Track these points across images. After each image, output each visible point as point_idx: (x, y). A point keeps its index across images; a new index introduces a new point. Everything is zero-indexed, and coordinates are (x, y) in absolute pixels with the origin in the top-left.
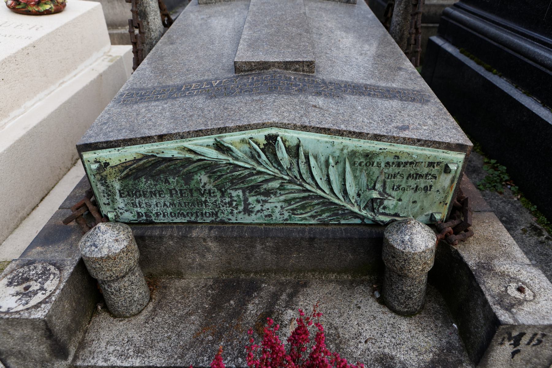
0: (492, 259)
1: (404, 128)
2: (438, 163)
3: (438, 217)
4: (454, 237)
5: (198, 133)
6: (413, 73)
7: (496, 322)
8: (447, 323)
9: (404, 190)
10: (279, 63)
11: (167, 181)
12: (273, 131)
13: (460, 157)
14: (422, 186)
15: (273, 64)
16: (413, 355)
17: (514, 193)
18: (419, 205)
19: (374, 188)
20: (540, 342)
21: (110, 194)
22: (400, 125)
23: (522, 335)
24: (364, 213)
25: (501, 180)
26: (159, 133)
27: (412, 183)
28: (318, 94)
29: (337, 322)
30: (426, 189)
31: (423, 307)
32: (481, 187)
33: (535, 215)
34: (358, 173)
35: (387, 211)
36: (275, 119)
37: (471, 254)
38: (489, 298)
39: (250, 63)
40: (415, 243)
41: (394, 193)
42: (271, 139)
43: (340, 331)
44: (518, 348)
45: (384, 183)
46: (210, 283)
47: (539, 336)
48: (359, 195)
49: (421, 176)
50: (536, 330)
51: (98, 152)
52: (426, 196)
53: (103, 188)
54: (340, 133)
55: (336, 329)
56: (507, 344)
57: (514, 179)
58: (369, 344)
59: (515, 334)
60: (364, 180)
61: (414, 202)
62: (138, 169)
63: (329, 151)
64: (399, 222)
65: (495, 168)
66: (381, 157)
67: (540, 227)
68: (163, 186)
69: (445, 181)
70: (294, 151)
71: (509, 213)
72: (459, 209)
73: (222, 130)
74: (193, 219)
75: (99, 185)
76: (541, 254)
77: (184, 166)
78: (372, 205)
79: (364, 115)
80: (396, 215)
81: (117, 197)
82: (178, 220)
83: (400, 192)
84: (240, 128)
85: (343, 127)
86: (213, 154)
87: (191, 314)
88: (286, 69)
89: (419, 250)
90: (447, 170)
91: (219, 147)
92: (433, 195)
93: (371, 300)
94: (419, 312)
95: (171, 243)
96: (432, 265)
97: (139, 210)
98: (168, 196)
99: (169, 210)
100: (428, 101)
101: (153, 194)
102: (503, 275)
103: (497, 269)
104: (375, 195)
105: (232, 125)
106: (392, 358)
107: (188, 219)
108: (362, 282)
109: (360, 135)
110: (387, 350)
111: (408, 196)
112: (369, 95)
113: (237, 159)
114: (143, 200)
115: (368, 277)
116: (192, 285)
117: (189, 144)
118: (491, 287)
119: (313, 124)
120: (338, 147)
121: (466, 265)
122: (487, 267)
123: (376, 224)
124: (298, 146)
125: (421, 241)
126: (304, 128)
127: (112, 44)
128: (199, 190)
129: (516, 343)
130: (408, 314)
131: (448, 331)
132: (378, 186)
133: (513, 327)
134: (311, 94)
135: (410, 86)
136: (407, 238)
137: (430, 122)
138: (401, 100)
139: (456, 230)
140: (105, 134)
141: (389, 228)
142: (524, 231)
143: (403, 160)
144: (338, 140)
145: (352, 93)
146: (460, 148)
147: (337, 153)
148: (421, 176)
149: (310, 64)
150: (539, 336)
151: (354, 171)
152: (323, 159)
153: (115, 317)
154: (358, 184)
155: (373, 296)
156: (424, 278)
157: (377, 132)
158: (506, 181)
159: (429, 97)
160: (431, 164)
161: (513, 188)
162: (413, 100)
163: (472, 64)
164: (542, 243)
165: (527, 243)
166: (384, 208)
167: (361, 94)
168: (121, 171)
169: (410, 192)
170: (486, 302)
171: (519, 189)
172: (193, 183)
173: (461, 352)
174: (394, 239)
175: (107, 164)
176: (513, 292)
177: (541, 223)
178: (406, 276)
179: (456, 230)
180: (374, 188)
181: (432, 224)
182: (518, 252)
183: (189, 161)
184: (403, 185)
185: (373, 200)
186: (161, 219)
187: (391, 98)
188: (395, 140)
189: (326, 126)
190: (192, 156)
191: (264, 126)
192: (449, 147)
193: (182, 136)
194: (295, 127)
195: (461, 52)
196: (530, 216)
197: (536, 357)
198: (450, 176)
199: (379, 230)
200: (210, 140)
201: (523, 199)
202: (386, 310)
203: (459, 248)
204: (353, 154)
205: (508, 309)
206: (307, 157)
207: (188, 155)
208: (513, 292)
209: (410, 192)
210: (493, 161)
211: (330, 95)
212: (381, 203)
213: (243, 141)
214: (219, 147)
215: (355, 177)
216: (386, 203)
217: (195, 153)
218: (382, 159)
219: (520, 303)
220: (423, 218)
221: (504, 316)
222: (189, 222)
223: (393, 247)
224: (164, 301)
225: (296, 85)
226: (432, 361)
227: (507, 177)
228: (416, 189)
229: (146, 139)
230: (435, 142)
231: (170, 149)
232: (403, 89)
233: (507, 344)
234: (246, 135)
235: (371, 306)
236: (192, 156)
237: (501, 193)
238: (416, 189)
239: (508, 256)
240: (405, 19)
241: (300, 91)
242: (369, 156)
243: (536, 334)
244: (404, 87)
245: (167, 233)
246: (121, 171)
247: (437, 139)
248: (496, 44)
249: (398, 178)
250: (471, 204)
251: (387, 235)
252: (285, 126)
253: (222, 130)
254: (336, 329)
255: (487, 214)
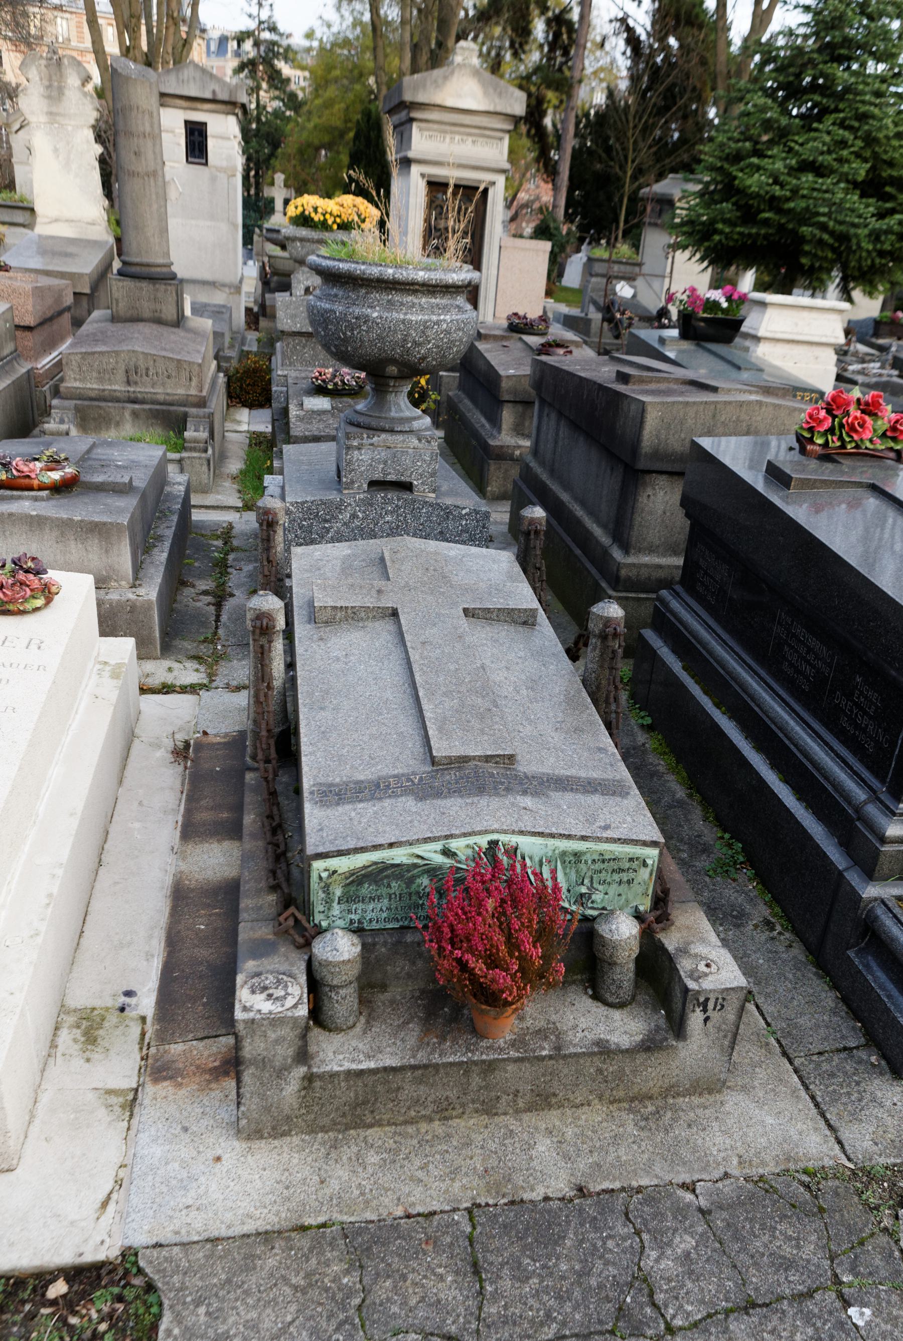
0: (689, 944)
1: (606, 828)
2: (637, 859)
3: (641, 908)
4: (655, 926)
5: (427, 840)
6: (613, 754)
7: (686, 990)
8: (655, 1010)
9: (609, 884)
10: (480, 756)
11: (389, 886)
12: (495, 837)
13: (655, 852)
14: (625, 879)
15: (474, 758)
16: (626, 1037)
17: (750, 880)
18: (624, 897)
19: (582, 884)
20: (723, 1006)
21: (328, 902)
22: (603, 824)
23: (707, 1000)
24: (574, 908)
25: (735, 863)
26: (389, 841)
27: (616, 877)
28: (525, 792)
29: (554, 1018)
30: (629, 882)
31: (633, 998)
32: (711, 873)
33: (770, 907)
34: (568, 870)
35: (595, 905)
36: (496, 826)
37: (671, 941)
38: (682, 973)
39: (450, 757)
40: (621, 931)
41: (601, 888)
42: (493, 844)
43: (558, 1025)
44: (708, 1014)
45: (592, 878)
46: (417, 994)
47: (720, 1000)
48: (569, 891)
49: (623, 870)
50: (716, 995)
51: (328, 860)
52: (630, 889)
53: (323, 895)
54: (552, 836)
55: (554, 1023)
56: (698, 1010)
57: (751, 861)
58: (586, 1033)
59: (702, 999)
60: (573, 876)
61: (620, 895)
62: (364, 876)
63: (542, 852)
64: (606, 914)
65: (730, 846)
66: (588, 855)
67: (773, 920)
68: (384, 891)
69: (644, 874)
70: (512, 852)
71: (741, 906)
72: (661, 900)
73: (447, 837)
74: (406, 923)
75: (320, 893)
76: (771, 952)
77: (408, 871)
78: (581, 899)
79: (568, 813)
80: (604, 908)
81: (335, 904)
82: (390, 926)
83: (606, 886)
84: (465, 835)
85: (554, 830)
86: (439, 859)
87: (408, 1023)
88: (487, 762)
89: (625, 937)
90: (645, 864)
91: (446, 852)
92: (637, 889)
93: (584, 997)
94: (630, 1004)
95: (383, 950)
96: (637, 951)
97: (353, 916)
98: (386, 901)
99: (384, 915)
100: (628, 793)
101: (372, 899)
102: (696, 955)
103: (692, 952)
104: (584, 890)
105: (457, 832)
106: (607, 1041)
107: (401, 923)
108: (574, 982)
109: (569, 837)
110: (602, 1036)
111: (613, 889)
112: (572, 790)
113: (460, 862)
114: (360, 906)
115: (579, 977)
116: (398, 997)
117: (420, 850)
118: (684, 965)
119: (528, 829)
120: (551, 848)
121: (666, 950)
122: (684, 951)
123: (586, 919)
124: (516, 849)
125: (623, 930)
126: (521, 833)
127: (103, 634)
128: (418, 893)
129: (705, 1010)
130: (621, 1006)
131: (656, 1017)
132: (586, 881)
133: (698, 992)
134: (518, 792)
135: (609, 775)
136: (614, 927)
137: (629, 819)
138: (603, 794)
139: (658, 920)
140: (331, 842)
141: (598, 920)
142: (756, 926)
143: (607, 857)
144: (551, 842)
145: (556, 790)
146: (654, 844)
147: (550, 854)
148: (623, 870)
149: (511, 758)
150: (720, 1000)
151: (564, 868)
152: (537, 859)
153: (330, 1031)
154: (568, 880)
155: (586, 993)
156: (632, 966)
157: (584, 833)
158: (741, 863)
159: (630, 787)
160: (631, 860)
161: (749, 873)
162: (614, 794)
163: (696, 690)
164: (773, 939)
165: (757, 940)
166: (593, 902)
167: (565, 789)
168: (347, 878)
169: (615, 886)
170: (680, 977)
171: (756, 874)
172: (414, 886)
173: (667, 1032)
174: (603, 929)
175: (335, 872)
176: (702, 967)
177: (775, 915)
178: (615, 964)
179: (658, 920)
180: (582, 884)
181: (638, 916)
182: (713, 938)
183: (415, 866)
184: (608, 880)
185: (582, 895)
186: (374, 925)
187: (592, 793)
188: (599, 839)
189: (540, 830)
190: (419, 861)
191: (486, 832)
192: (645, 844)
193: (411, 844)
194: (513, 832)
195: (684, 668)
196: (764, 907)
197: (724, 1023)
198: (648, 870)
199: (589, 924)
200: (438, 846)
201: (760, 886)
202: (600, 1004)
203: (661, 936)
204: (564, 854)
205: (696, 980)
206: (523, 858)
207: (416, 861)
208: (702, 967)
209: (615, 886)
210: (727, 836)
211: (536, 794)
212: (590, 897)
213: (468, 846)
214: (446, 852)
215: (565, 874)
216: (593, 897)
217: (422, 858)
218: (588, 857)
219: (706, 975)
220: (629, 910)
221: (692, 985)
222: (402, 928)
223: (602, 937)
224: (374, 1014)
225: (502, 783)
226: (642, 1041)
227: (741, 859)
228: (620, 883)
229: (376, 847)
230: (633, 840)
231: (399, 856)
232: (604, 780)
233: (698, 1010)
234: (471, 840)
235: (585, 1002)
236: (419, 861)
237: (734, 880)
238: (620, 883)
239: (703, 940)
240: (601, 667)
241: (508, 790)
242: (577, 855)
243: (717, 999)
244: (605, 776)
245: (380, 939)
246: (347, 878)
247: (634, 837)
248: (722, 672)
249: (604, 874)
250: (673, 896)
251: (596, 926)
252: (505, 832)
253: (447, 837)
254: (554, 1023)
255: (691, 904)
